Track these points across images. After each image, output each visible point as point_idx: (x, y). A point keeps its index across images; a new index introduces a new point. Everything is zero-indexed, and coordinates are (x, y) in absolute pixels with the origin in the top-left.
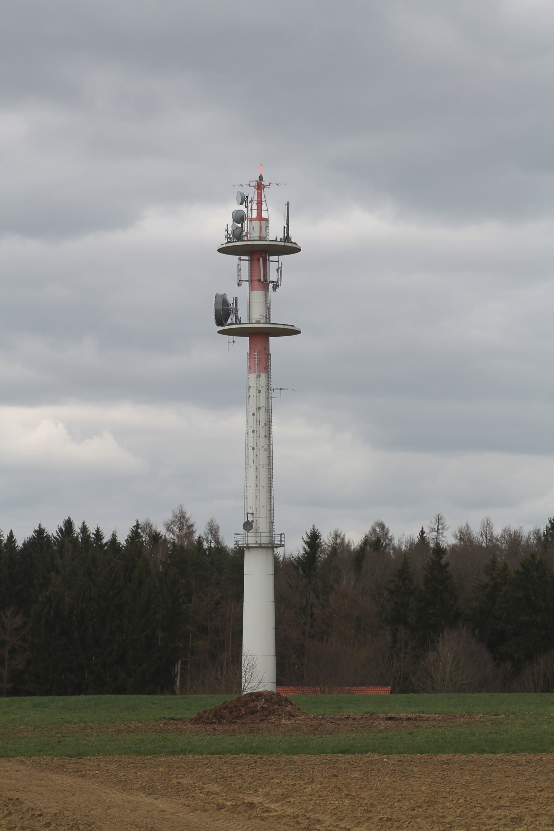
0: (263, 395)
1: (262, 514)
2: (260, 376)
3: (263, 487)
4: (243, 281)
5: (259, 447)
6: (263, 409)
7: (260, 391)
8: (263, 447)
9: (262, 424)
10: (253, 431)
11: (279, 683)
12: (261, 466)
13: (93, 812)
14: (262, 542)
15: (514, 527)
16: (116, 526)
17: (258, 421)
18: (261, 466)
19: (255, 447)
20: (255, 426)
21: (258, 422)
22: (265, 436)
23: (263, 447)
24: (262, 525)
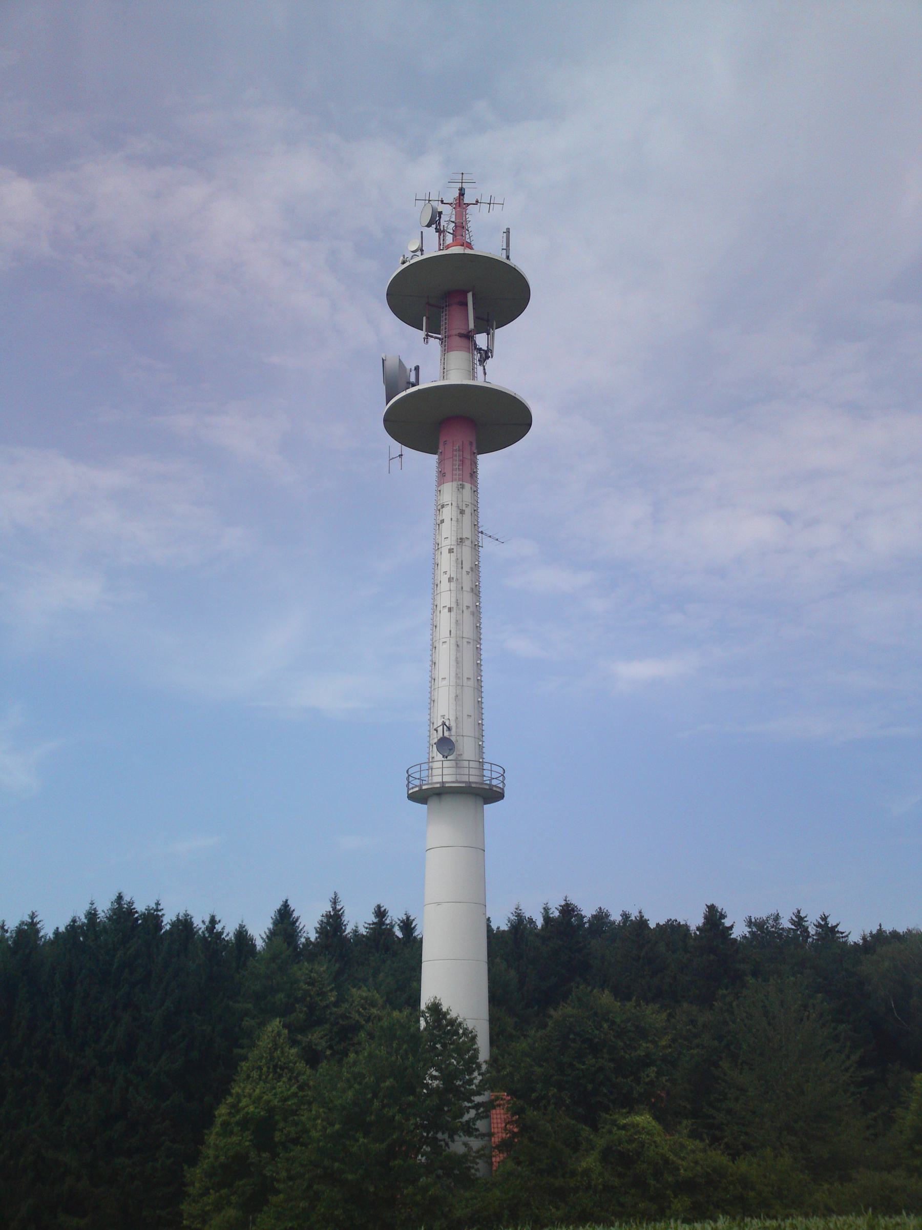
0: (467, 518)
1: (468, 728)
2: (463, 487)
3: (468, 679)
4: (450, 204)
5: (461, 607)
6: (468, 543)
7: (462, 512)
8: (468, 607)
9: (467, 567)
10: (450, 580)
11: (434, 452)
12: (465, 640)
13: (701, 1145)
14: (446, 779)
15: (761, 913)
16: (854, 930)
17: (460, 560)
18: (465, 640)
19: (454, 605)
20: (453, 569)
21: (460, 563)
22: (472, 590)
23: (468, 607)
24: (467, 748)
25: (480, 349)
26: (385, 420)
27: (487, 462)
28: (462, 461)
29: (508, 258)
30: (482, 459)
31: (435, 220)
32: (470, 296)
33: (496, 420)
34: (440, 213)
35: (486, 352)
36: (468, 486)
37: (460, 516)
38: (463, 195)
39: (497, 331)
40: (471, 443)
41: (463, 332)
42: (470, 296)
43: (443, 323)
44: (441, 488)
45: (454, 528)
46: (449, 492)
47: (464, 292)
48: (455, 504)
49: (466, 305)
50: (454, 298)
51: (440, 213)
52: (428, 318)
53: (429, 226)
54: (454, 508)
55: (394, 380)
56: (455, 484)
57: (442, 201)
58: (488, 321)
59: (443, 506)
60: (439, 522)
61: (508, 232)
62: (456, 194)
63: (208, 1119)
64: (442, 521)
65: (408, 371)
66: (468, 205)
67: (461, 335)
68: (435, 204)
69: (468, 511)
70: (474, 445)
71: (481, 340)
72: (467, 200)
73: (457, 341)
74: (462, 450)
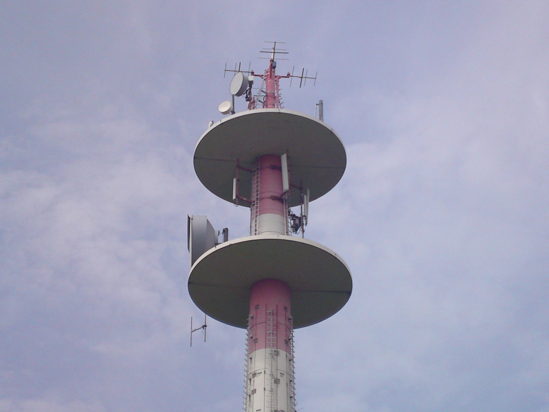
2: (277, 354)
7: (277, 381)
25: (294, 216)
26: (349, 293)
27: (301, 335)
28: (277, 326)
29: (321, 116)
30: (299, 334)
31: (246, 89)
32: (284, 159)
33: (309, 286)
34: (251, 83)
35: (300, 219)
36: (283, 353)
37: (274, 386)
38: (274, 67)
39: (310, 204)
40: (285, 308)
41: (276, 195)
42: (284, 159)
43: (254, 186)
44: (252, 355)
45: (268, 399)
46: (261, 360)
47: (274, 154)
48: (268, 372)
49: (280, 169)
50: (269, 161)
51: (251, 83)
52: (238, 181)
53: (239, 94)
54: (268, 376)
55: (198, 240)
56: (268, 350)
57: (252, 73)
58: (301, 189)
59: (254, 375)
60: (250, 392)
61: (321, 104)
62: (268, 66)
63: (293, 322)
64: (254, 391)
65: (217, 233)
66: (280, 77)
67: (274, 198)
68: (246, 75)
69: (283, 381)
70: (289, 311)
71: (296, 210)
72: (278, 72)
73: (270, 203)
74: (276, 314)
